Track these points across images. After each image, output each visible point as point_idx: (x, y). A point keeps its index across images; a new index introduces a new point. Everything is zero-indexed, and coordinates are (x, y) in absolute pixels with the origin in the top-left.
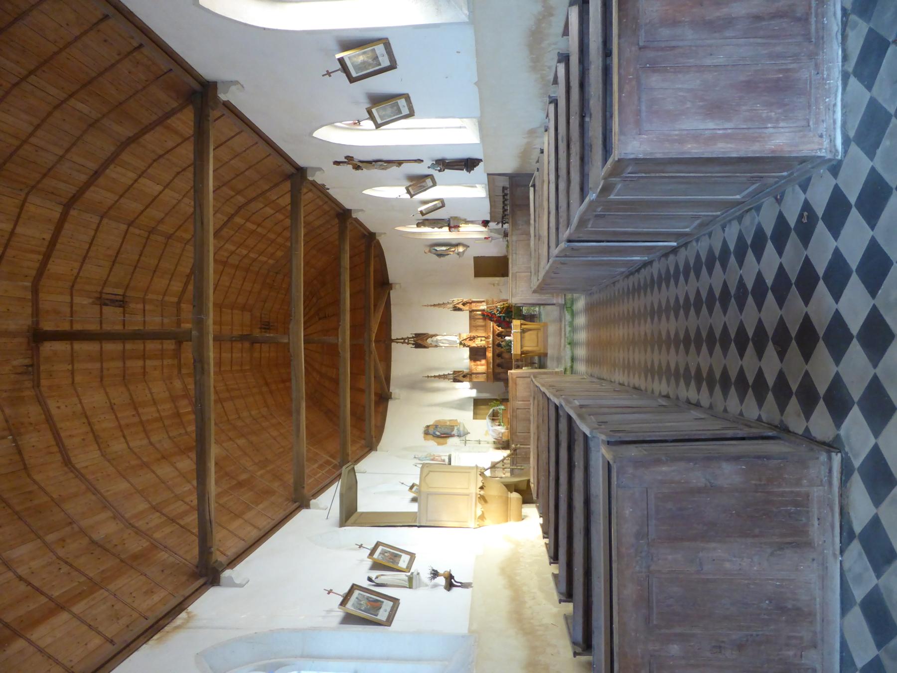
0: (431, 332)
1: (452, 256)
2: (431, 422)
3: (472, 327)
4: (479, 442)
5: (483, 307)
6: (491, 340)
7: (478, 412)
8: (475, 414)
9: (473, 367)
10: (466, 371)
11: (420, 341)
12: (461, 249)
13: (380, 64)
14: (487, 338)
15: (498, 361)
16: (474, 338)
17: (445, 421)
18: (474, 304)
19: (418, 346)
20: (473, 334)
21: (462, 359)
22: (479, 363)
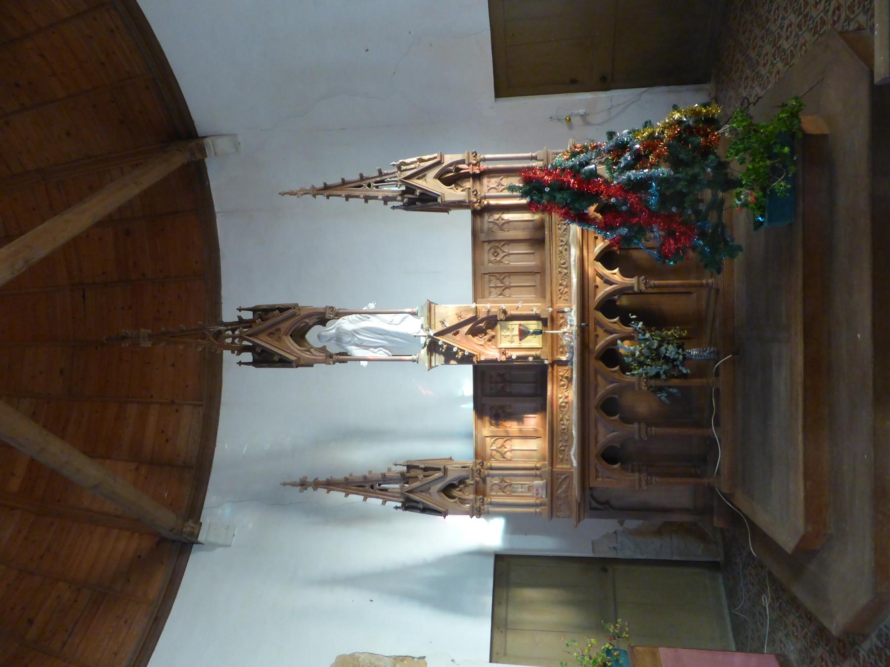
0: (311, 300)
3: (483, 278)
7: (513, 615)
8: (499, 625)
9: (492, 446)
11: (284, 335)
13: (520, 325)
14: (548, 321)
15: (606, 433)
19: (264, 359)
20: (487, 307)
21: (441, 414)
22: (512, 426)
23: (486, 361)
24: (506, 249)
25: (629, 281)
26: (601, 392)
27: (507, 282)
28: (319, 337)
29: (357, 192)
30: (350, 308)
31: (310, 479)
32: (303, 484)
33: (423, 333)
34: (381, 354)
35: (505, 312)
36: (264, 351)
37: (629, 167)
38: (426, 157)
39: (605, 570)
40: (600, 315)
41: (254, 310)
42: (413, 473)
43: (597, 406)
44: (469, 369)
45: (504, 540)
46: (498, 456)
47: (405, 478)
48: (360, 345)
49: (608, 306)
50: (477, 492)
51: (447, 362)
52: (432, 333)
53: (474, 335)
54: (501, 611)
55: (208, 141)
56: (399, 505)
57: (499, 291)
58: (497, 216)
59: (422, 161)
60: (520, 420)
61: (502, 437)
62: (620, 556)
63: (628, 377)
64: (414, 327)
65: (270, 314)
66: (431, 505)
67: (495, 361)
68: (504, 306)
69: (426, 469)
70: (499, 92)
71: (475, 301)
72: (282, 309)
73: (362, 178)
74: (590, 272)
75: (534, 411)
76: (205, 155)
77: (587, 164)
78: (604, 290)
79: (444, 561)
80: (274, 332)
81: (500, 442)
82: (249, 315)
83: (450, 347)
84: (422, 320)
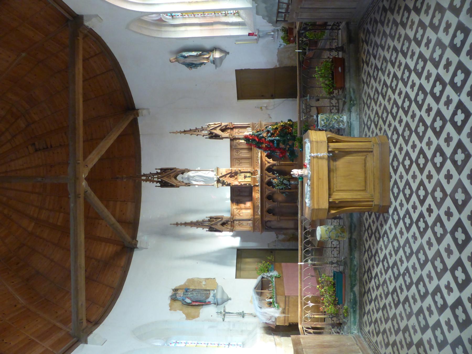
0: (181, 167)
1: (207, 69)
2: (180, 282)
3: (234, 160)
4: (242, 315)
5: (248, 132)
6: (258, 176)
7: (243, 266)
8: (238, 269)
9: (236, 212)
10: (227, 215)
11: (168, 178)
12: (217, 55)
14: (253, 173)
15: (268, 205)
16: (236, 173)
17: (199, 281)
18: (236, 130)
19: (164, 184)
20: (235, 169)
21: (220, 201)
22: (242, 206)
23: (235, 185)
24: (241, 151)
25: (275, 162)
26: (267, 193)
27: (241, 161)
28: (182, 178)
29: (195, 133)
30: (191, 169)
31: (179, 223)
32: (177, 224)
33: (215, 177)
34: (202, 183)
35: (240, 171)
36: (166, 182)
37: (270, 137)
38: (216, 123)
39: (272, 252)
40: (266, 172)
41: (161, 169)
42: (212, 220)
43: (267, 197)
44: (229, 188)
45: (240, 244)
46: (238, 215)
47: (209, 221)
48: (195, 181)
49: (270, 169)
50: (231, 226)
51: (223, 186)
52: (218, 177)
53: (231, 177)
54: (239, 265)
55: (140, 111)
56: (208, 230)
57: (238, 164)
58: (238, 141)
59: (215, 124)
60: (245, 203)
61: (239, 209)
62: (277, 248)
63: (274, 189)
64: (212, 175)
65: (167, 171)
66: (218, 229)
67: (237, 185)
68: (240, 169)
69: (216, 218)
70: (239, 98)
71: (231, 167)
72: (171, 169)
73: (196, 129)
74: (264, 160)
75: (249, 201)
76: (138, 116)
77: (261, 134)
78: (268, 165)
79: (220, 251)
80: (169, 176)
81: (239, 210)
82: (159, 171)
83: (224, 181)
84: (215, 173)
